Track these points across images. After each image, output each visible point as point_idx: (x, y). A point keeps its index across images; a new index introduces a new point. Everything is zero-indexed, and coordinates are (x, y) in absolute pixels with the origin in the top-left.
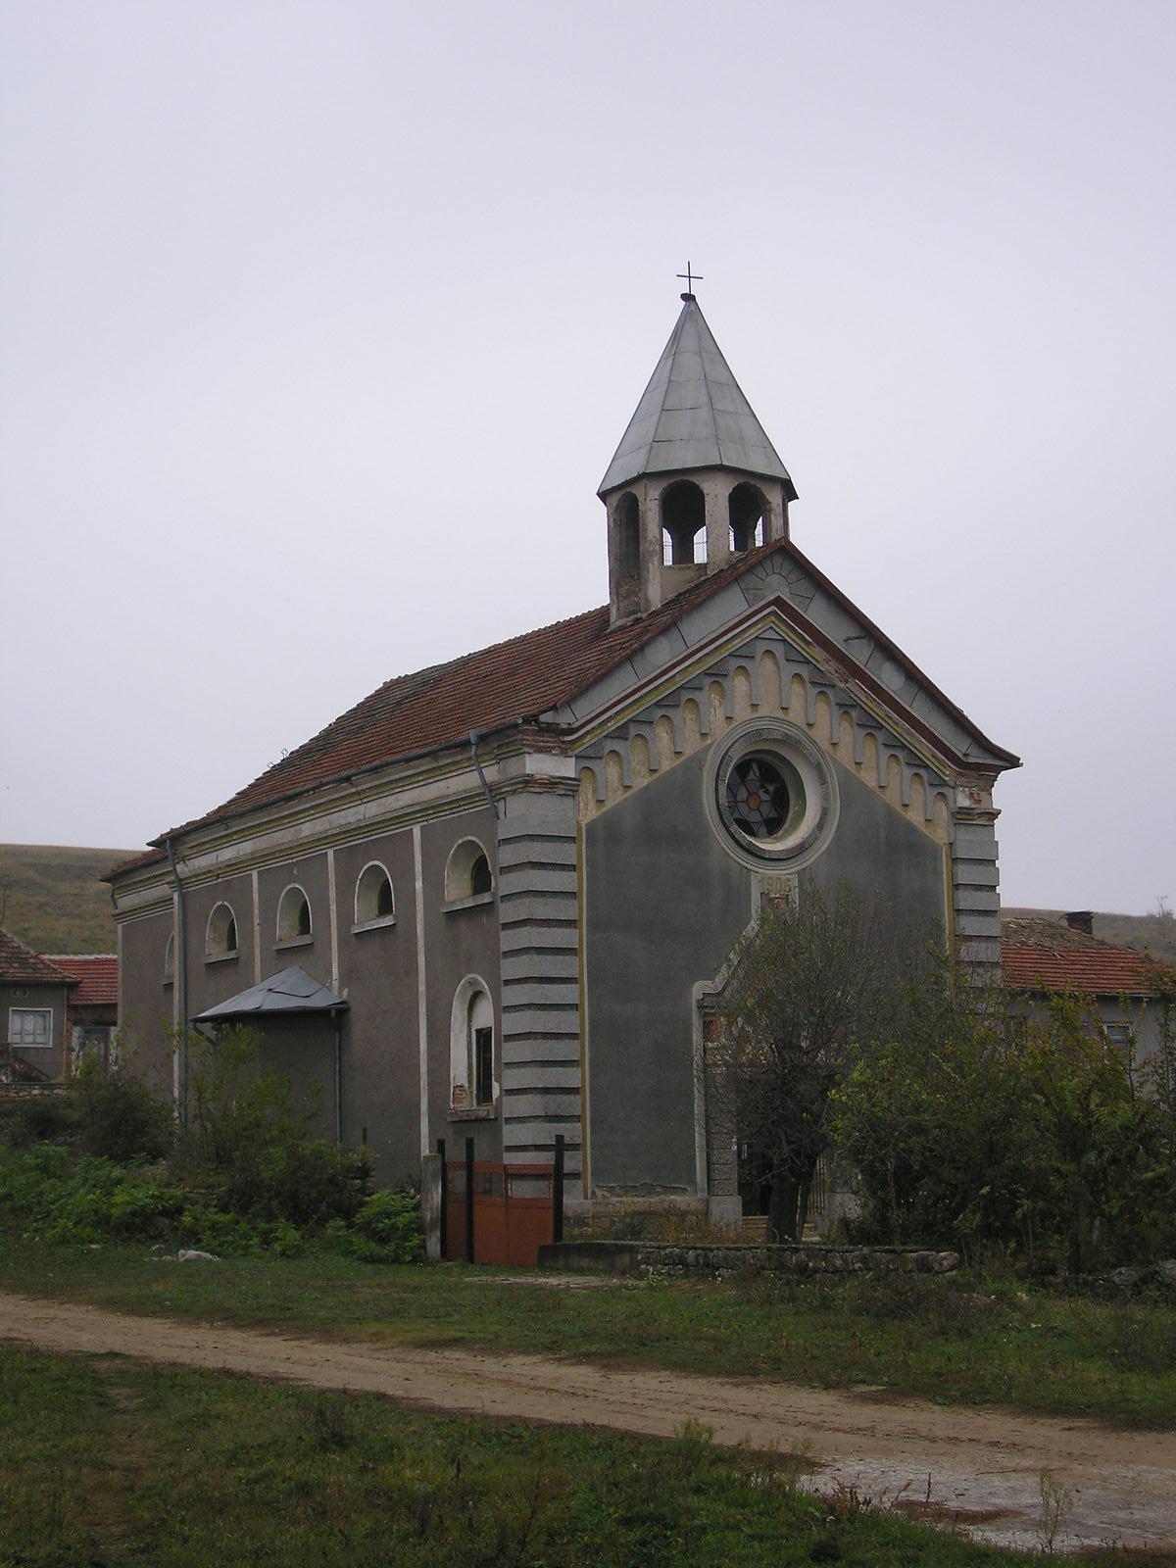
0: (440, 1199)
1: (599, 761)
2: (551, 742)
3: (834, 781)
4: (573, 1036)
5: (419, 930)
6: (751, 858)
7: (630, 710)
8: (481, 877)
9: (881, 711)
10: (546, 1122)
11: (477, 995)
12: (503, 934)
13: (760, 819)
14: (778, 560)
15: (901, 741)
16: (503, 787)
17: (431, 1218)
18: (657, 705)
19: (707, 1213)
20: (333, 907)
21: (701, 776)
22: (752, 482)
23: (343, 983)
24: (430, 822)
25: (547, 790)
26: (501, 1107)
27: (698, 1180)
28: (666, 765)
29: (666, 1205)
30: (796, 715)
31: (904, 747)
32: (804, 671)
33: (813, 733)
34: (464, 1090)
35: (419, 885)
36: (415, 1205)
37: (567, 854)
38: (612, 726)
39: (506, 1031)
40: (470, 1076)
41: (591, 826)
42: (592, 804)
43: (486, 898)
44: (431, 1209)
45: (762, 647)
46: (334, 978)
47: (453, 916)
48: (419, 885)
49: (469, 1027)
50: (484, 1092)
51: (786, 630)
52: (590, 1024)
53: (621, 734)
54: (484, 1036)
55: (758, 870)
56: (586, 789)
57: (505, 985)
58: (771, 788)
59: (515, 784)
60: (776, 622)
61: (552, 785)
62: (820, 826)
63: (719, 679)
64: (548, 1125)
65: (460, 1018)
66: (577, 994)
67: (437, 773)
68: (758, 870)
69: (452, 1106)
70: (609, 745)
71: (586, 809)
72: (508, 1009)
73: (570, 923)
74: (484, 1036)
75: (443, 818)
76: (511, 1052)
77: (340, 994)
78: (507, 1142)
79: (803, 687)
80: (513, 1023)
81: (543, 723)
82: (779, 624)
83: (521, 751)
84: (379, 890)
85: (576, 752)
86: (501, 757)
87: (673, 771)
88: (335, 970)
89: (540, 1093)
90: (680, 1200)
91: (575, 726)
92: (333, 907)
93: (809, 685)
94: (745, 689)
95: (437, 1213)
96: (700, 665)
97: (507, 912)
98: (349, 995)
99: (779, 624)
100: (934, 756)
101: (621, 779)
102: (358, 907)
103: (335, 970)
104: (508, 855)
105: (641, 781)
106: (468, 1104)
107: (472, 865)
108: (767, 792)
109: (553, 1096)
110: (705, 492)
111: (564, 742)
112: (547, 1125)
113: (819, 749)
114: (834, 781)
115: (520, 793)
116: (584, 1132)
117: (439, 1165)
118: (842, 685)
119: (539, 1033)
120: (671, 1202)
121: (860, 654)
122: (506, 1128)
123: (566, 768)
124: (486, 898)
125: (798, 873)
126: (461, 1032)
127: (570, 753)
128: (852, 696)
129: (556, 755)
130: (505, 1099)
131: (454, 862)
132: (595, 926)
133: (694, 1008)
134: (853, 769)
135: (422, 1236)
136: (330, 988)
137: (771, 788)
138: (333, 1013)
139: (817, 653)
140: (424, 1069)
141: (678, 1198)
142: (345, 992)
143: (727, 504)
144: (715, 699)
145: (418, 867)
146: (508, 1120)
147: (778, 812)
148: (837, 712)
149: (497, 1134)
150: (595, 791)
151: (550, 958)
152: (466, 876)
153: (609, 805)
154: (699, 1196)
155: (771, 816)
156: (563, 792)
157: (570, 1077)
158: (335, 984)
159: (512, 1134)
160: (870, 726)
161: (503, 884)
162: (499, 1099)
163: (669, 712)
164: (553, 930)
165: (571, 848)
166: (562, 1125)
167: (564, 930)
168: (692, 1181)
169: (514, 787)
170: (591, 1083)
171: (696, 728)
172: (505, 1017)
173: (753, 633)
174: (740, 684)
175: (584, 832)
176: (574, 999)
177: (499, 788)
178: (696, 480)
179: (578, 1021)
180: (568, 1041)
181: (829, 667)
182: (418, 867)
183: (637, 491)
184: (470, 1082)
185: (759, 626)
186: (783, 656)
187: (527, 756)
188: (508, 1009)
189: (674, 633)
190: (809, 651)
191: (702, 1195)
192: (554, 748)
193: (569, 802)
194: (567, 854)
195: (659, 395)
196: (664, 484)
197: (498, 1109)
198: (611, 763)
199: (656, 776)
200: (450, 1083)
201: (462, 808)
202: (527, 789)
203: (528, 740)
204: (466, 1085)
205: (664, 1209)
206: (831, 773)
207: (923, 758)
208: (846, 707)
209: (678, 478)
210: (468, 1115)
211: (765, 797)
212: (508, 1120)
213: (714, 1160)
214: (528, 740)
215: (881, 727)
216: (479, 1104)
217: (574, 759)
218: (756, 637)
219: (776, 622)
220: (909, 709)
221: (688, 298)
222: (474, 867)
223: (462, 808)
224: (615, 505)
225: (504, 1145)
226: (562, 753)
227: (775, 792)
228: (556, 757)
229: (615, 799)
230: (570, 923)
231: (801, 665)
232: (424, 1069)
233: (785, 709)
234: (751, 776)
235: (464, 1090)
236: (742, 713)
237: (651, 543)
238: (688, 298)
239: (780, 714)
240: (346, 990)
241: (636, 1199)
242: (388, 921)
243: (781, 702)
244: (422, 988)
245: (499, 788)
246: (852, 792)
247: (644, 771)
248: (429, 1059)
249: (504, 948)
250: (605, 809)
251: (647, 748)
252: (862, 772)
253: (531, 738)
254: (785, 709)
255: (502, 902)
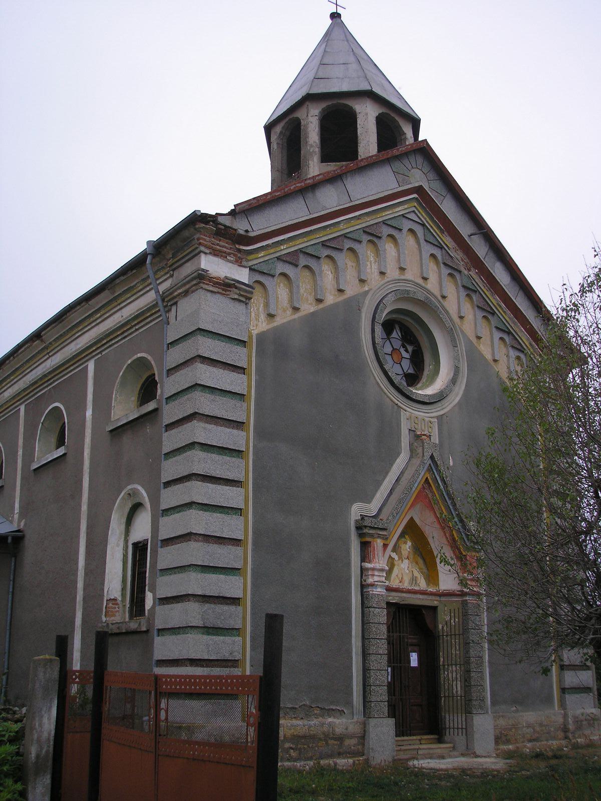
0: (53, 727)
1: (270, 278)
2: (225, 247)
3: (462, 347)
4: (236, 542)
5: (86, 454)
6: (400, 396)
7: (300, 241)
8: (148, 390)
9: (494, 300)
10: (203, 634)
11: (137, 507)
12: (165, 435)
13: (401, 372)
14: (420, 159)
15: (508, 328)
16: (176, 290)
17: (38, 756)
18: (324, 244)
19: (363, 737)
20: (20, 452)
21: (360, 316)
22: (393, 115)
23: (22, 515)
24: (103, 353)
25: (220, 291)
26: (154, 619)
27: (355, 703)
28: (331, 299)
29: (325, 729)
30: (432, 285)
31: (509, 333)
32: (438, 253)
33: (446, 304)
34: (117, 604)
35: (89, 413)
36: (17, 732)
37: (237, 355)
38: (285, 249)
39: (164, 534)
40: (124, 589)
41: (261, 337)
42: (263, 317)
43: (151, 406)
44: (39, 741)
45: (406, 225)
46: (16, 512)
47: (117, 432)
48: (89, 413)
49: (126, 541)
50: (137, 605)
51: (425, 216)
52: (254, 533)
53: (291, 259)
54: (140, 549)
55: (408, 409)
56: (258, 300)
57: (165, 488)
58: (410, 348)
59: (188, 282)
60: (418, 208)
61: (226, 286)
62: (454, 381)
63: (375, 240)
64: (206, 638)
65: (118, 532)
66: (242, 498)
67: (113, 305)
68: (408, 409)
69: (104, 619)
70: (281, 268)
71: (257, 320)
72: (167, 512)
73: (238, 425)
74: (140, 549)
75: (116, 346)
76: (167, 557)
77: (19, 525)
78: (158, 655)
79: (437, 267)
80: (170, 526)
81: (221, 224)
82: (420, 210)
83: (197, 251)
84: (57, 434)
85: (250, 263)
86: (174, 267)
87: (335, 306)
88: (17, 506)
89: (199, 601)
90: (340, 724)
91: (252, 234)
92: (20, 452)
93: (442, 265)
94: (394, 254)
95: (48, 748)
96: (359, 221)
97: (170, 413)
98: (25, 525)
99: (420, 210)
100: (531, 345)
101: (291, 300)
102: (39, 447)
103: (17, 506)
104: (175, 356)
105: (308, 307)
106: (120, 617)
107: (139, 386)
108: (407, 351)
109: (213, 606)
110: (358, 111)
111: (239, 251)
112: (205, 637)
113: (451, 320)
114: (462, 347)
115: (193, 292)
116: (244, 648)
117: (56, 674)
118: (466, 272)
119: (200, 534)
120: (330, 724)
121: (480, 249)
122: (158, 640)
123: (242, 275)
124: (151, 406)
125: (437, 417)
126: (118, 545)
127: (244, 263)
128: (474, 283)
129: (230, 262)
130: (158, 608)
131: (123, 383)
132: (261, 434)
133: (353, 528)
134: (474, 340)
135: (19, 786)
136: (11, 522)
137: (410, 348)
138: (10, 540)
139: (448, 241)
140: (80, 585)
141: (337, 721)
142: (22, 524)
143: (375, 122)
144: (371, 257)
145: (90, 397)
146: (161, 631)
147: (415, 371)
148: (463, 293)
149: (148, 647)
150: (267, 305)
151: (215, 456)
152: (133, 399)
153: (279, 321)
154: (355, 719)
155: (410, 371)
156: (236, 297)
157: (231, 586)
158: (16, 516)
159: (164, 648)
160: (488, 312)
161: (167, 386)
162: (153, 607)
163: (333, 254)
164: (220, 428)
165: (242, 351)
166: (222, 638)
167: (230, 430)
168: (349, 703)
169: (187, 286)
170: (253, 594)
171: (356, 275)
172: (164, 521)
173: (400, 210)
174: (389, 249)
175: (254, 341)
176: (238, 503)
177: (171, 294)
178: (350, 103)
179: (242, 527)
180: (230, 547)
181: (458, 255)
182: (90, 397)
183: (300, 114)
184: (123, 595)
185: (406, 206)
186: (423, 238)
187: (203, 256)
188: (167, 512)
189: (340, 184)
190: (442, 237)
191: (359, 717)
192: (229, 254)
193: (241, 307)
194: (237, 355)
195: (316, 62)
196: (324, 105)
197: (151, 621)
198: (282, 285)
199: (321, 306)
200: (104, 595)
201: (134, 329)
202: (201, 285)
203: (205, 240)
204: (120, 599)
205: (324, 733)
206: (459, 340)
207: (523, 344)
208: (470, 291)
209: (335, 102)
210: (118, 628)
211: (405, 354)
212: (161, 631)
213: (372, 681)
214: (205, 240)
215: (493, 314)
216: (131, 617)
217: (248, 268)
218: (403, 216)
219: (418, 208)
220: (514, 300)
221: (335, 16)
222: (141, 388)
223: (134, 329)
224: (279, 132)
225: (160, 538)
226: (237, 261)
227: (413, 351)
228: (231, 265)
229: (284, 317)
230: (238, 425)
231: (436, 248)
232: (80, 585)
233: (425, 279)
234: (394, 335)
235: (117, 604)
236: (393, 273)
237: (311, 146)
238: (335, 16)
239: (421, 281)
240: (24, 520)
241: (295, 722)
242: (61, 451)
243: (422, 273)
244: (84, 508)
245: (171, 294)
246: (474, 359)
247: (311, 299)
248: (86, 574)
249: (166, 450)
250: (275, 324)
251: (315, 281)
252: (481, 346)
253: (208, 239)
254: (425, 279)
255: (167, 404)
